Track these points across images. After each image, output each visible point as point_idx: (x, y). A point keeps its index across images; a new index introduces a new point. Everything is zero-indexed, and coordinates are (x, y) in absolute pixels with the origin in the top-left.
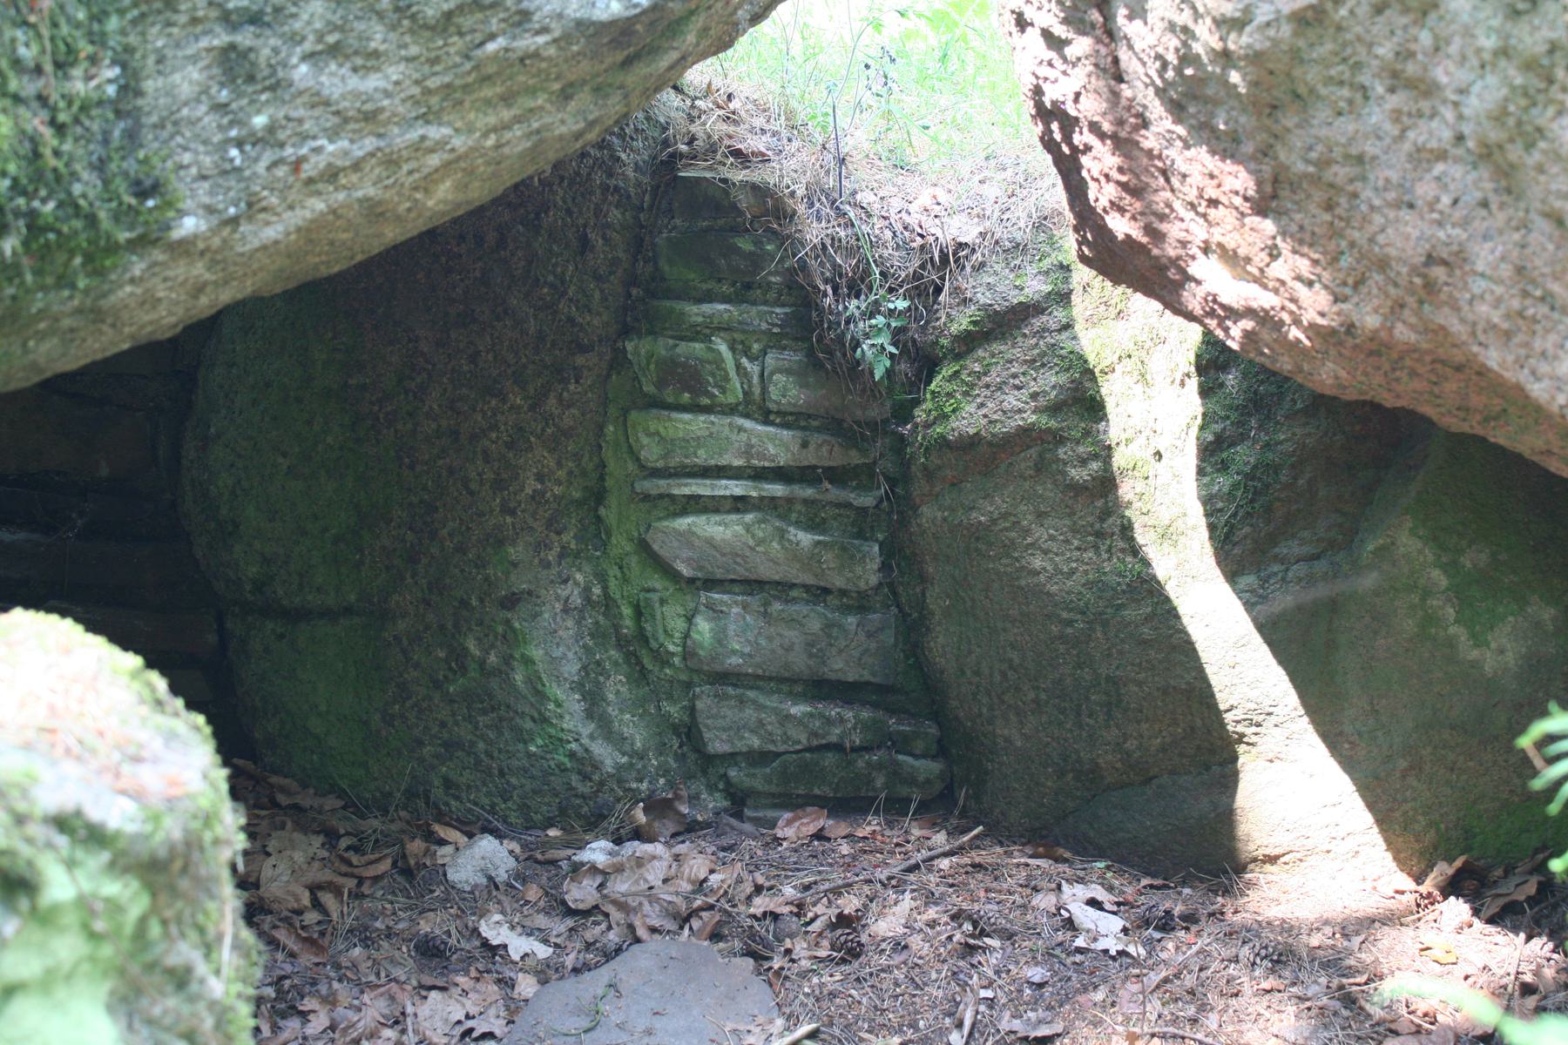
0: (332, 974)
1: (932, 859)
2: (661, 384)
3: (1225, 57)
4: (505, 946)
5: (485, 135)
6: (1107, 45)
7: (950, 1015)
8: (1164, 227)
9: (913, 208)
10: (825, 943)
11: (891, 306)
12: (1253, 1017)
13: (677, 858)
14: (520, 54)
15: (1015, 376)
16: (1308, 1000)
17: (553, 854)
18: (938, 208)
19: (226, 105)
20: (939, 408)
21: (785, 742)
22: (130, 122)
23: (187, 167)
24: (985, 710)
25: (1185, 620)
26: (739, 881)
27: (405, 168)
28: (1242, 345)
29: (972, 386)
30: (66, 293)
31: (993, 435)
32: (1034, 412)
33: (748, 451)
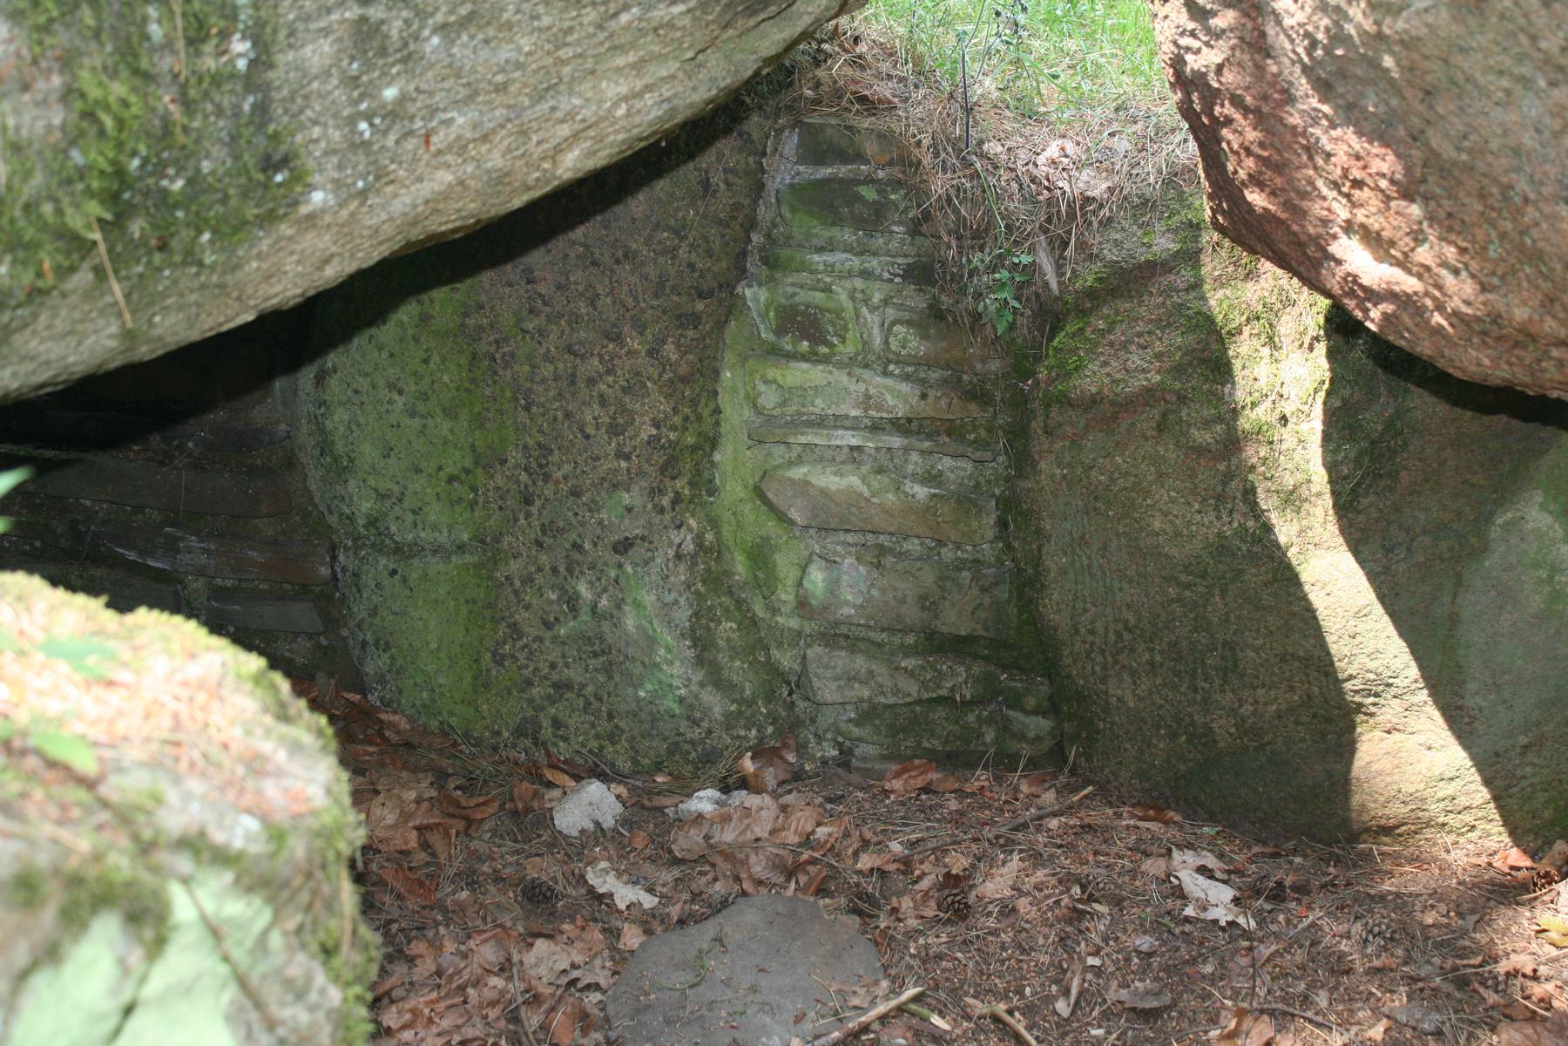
0: (439, 918)
1: (1040, 818)
2: (780, 331)
4: (611, 895)
5: (616, 105)
6: (1254, 20)
7: (1057, 982)
8: (1305, 204)
9: (1041, 160)
10: (933, 903)
11: (1016, 260)
12: (1364, 996)
13: (784, 808)
14: (654, 24)
15: (1140, 335)
16: (1420, 980)
17: (659, 801)
18: (1066, 161)
19: (357, 78)
20: (1062, 365)
21: (894, 695)
22: (260, 96)
23: (317, 141)
24: (1098, 669)
25: (1307, 588)
26: (847, 835)
27: (535, 138)
28: (1380, 327)
29: (1097, 345)
30: (193, 270)
31: (1117, 395)
32: (1158, 372)
33: (866, 401)
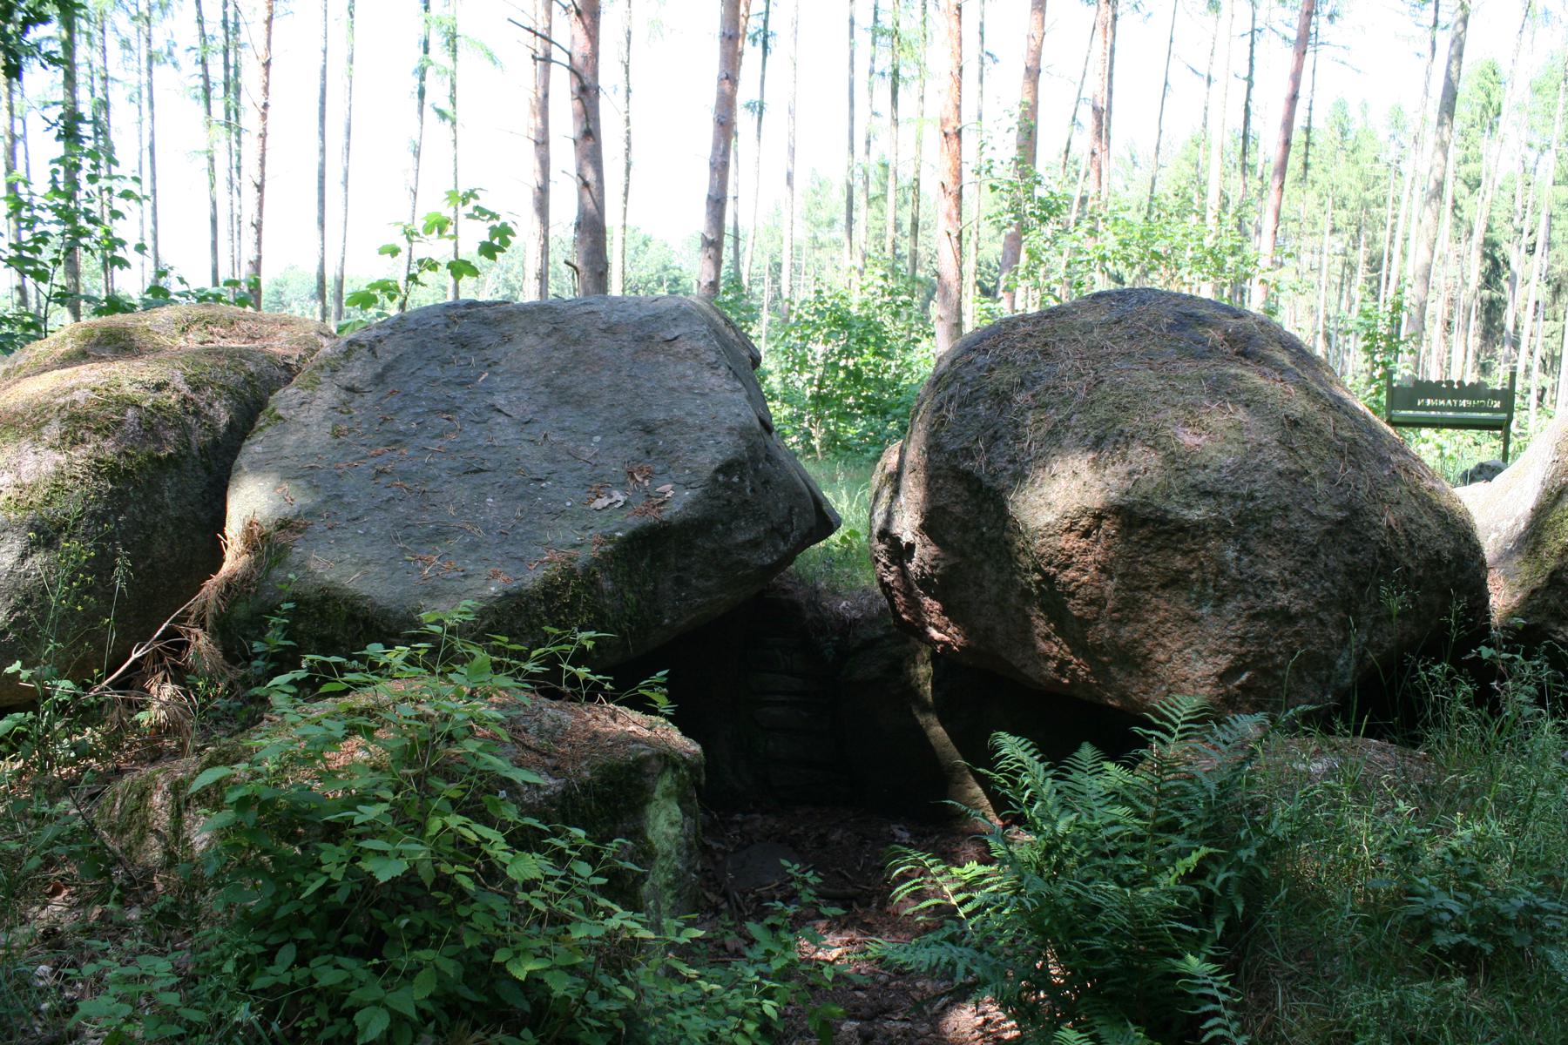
3: (932, 575)
